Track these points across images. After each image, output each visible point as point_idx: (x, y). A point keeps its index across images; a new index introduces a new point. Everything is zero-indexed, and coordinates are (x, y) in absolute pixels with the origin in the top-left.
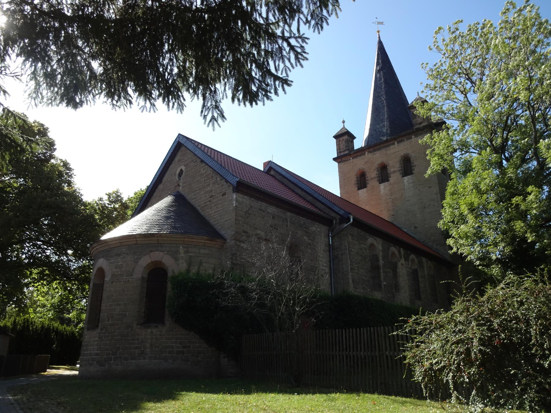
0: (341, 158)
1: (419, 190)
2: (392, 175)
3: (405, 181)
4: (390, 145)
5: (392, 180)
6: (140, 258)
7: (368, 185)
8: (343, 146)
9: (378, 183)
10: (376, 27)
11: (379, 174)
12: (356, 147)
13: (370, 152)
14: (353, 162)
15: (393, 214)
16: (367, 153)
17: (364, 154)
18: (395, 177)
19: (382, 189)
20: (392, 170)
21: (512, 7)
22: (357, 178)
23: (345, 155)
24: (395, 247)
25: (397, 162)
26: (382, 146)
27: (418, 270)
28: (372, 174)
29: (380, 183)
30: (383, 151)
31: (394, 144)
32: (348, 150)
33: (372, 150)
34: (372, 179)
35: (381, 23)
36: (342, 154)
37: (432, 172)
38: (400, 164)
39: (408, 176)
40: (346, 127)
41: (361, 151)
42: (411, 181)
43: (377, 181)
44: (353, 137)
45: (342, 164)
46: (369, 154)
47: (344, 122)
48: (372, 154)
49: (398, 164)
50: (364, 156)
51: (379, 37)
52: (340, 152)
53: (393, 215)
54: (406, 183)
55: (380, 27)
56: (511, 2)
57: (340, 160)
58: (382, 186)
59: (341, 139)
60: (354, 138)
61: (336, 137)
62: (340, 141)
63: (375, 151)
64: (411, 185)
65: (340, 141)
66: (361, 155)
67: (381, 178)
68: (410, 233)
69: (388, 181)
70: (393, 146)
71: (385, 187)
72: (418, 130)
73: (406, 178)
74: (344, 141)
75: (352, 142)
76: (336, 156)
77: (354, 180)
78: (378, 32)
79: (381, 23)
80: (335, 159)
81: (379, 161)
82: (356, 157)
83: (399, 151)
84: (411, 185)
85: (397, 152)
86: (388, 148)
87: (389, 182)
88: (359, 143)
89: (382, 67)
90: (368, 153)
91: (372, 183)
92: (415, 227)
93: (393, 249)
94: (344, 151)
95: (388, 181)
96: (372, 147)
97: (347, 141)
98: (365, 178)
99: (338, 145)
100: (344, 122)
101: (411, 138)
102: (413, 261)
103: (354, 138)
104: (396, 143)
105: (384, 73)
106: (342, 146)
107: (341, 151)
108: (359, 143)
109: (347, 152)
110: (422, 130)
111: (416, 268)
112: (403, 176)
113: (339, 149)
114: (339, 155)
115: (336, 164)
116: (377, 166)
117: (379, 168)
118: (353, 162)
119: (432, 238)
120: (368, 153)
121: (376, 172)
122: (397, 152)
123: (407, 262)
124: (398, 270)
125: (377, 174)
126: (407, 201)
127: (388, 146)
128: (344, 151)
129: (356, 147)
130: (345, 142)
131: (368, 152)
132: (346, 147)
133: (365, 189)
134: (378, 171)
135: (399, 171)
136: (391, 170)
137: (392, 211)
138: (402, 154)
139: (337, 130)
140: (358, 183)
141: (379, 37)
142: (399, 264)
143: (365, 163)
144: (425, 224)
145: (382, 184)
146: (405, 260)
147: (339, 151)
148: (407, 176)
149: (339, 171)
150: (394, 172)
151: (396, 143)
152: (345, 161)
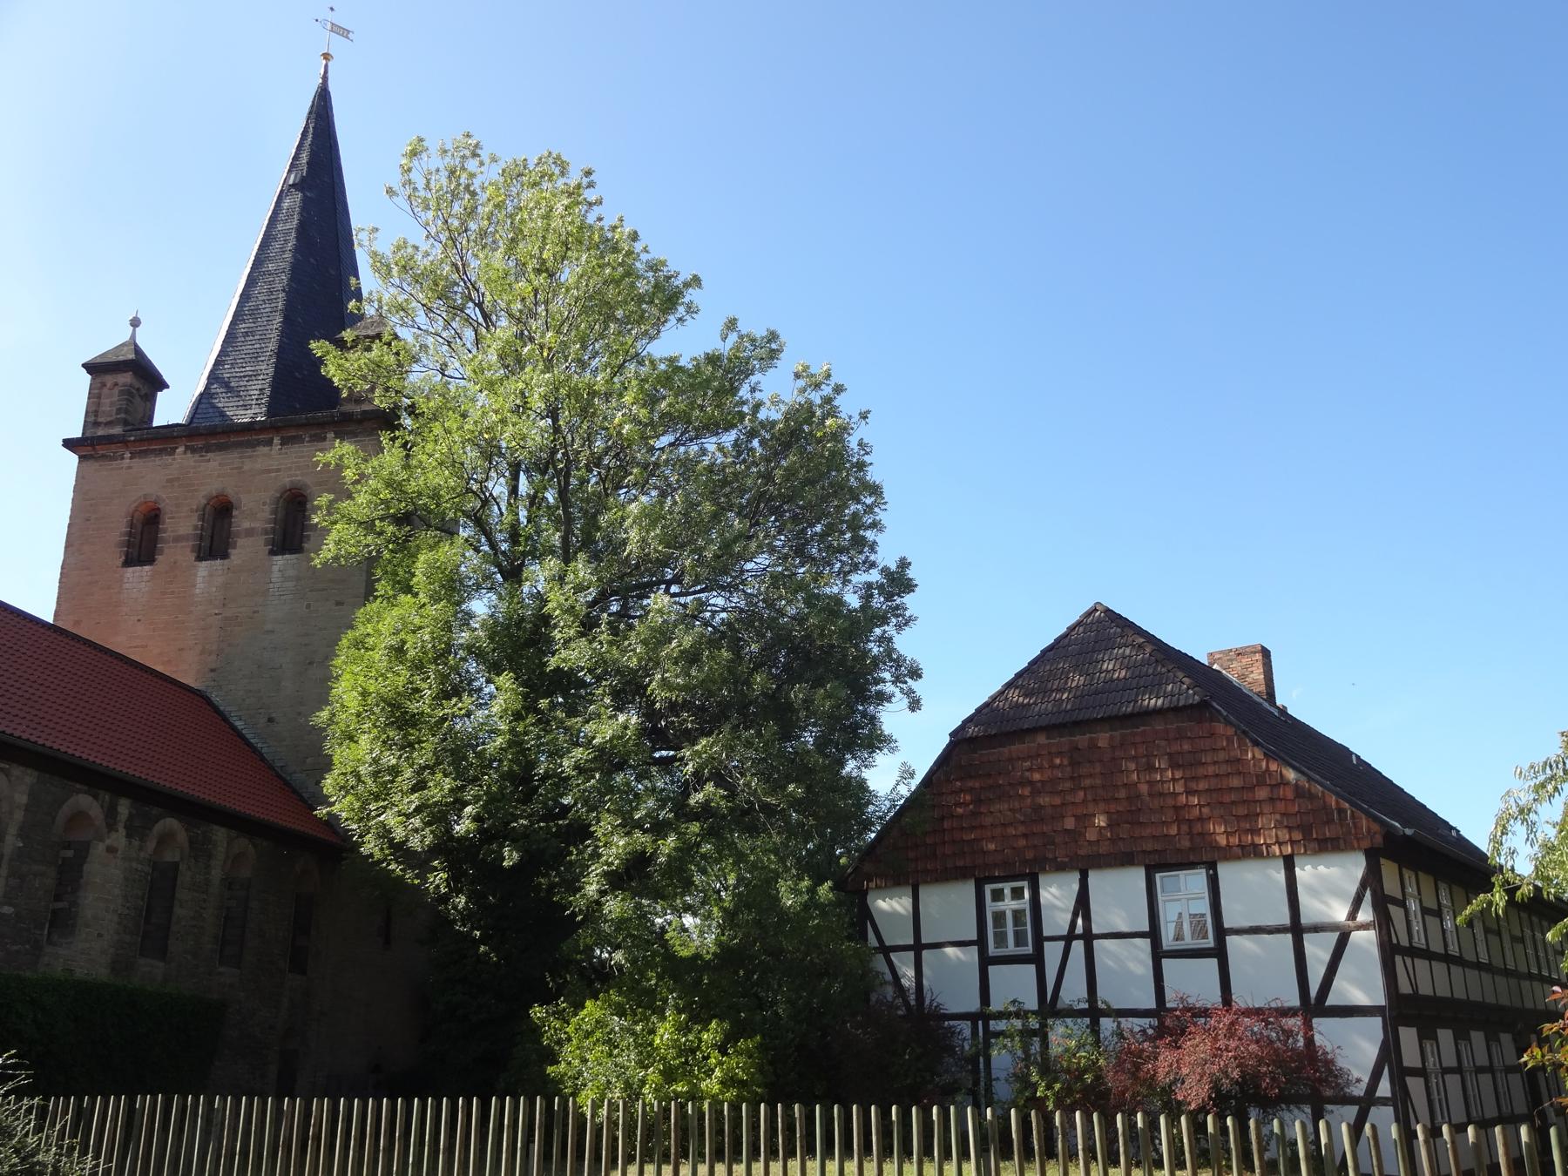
0: (92, 445)
1: (308, 606)
2: (240, 542)
3: (275, 568)
4: (259, 443)
5: (237, 556)
6: (102, 807)
7: (159, 558)
8: (112, 404)
9: (193, 557)
10: (326, 40)
11: (202, 528)
12: (159, 420)
13: (193, 450)
14: (130, 468)
15: (213, 666)
16: (181, 449)
17: (172, 451)
18: (248, 549)
19: (199, 580)
20: (246, 525)
21: (557, 171)
22: (131, 525)
23: (109, 440)
24: (96, 797)
25: (264, 504)
26: (233, 439)
27: (182, 867)
28: (181, 524)
29: (199, 558)
30: (233, 457)
31: (269, 443)
32: (125, 423)
33: (199, 443)
34: (177, 539)
35: (344, 33)
36: (101, 432)
37: (336, 558)
38: (275, 512)
39: (287, 556)
40: (139, 342)
41: (171, 434)
42: (291, 573)
43: (192, 551)
44: (157, 383)
45: (93, 466)
46: (189, 455)
47: (135, 323)
48: (197, 457)
49: (267, 508)
50: (169, 459)
51: (325, 78)
52: (96, 424)
53: (212, 670)
54: (276, 576)
55: (337, 45)
56: (558, 157)
57: (87, 451)
58: (204, 568)
59: (109, 379)
60: (162, 385)
61: (91, 367)
62: (104, 385)
63: (208, 449)
64: (290, 584)
65: (104, 385)
66: (161, 452)
67: (206, 544)
68: (248, 736)
69: (225, 556)
70: (264, 450)
71: (211, 575)
72: (348, 418)
73: (279, 560)
74: (116, 391)
75: (150, 400)
76: (77, 432)
77: (118, 529)
78: (326, 56)
79: (344, 33)
80: (69, 444)
81: (212, 486)
82: (143, 454)
83: (278, 470)
84: (290, 584)
85: (269, 471)
86: (249, 452)
87: (226, 562)
88: (171, 409)
89: (303, 179)
90: (185, 452)
91: (176, 552)
92: (271, 720)
93: (84, 801)
94: (109, 424)
95: (225, 556)
96: (201, 435)
97: (130, 393)
98: (157, 531)
99: (95, 396)
100: (135, 323)
101: (324, 439)
102: (165, 839)
103: (162, 385)
104: (276, 441)
105: (305, 200)
106: (108, 406)
107: (100, 420)
108: (171, 409)
109: (117, 430)
110: (360, 422)
111: (177, 859)
112: (272, 553)
113: (96, 413)
114: (88, 435)
115: (73, 459)
116: (204, 501)
117: (209, 507)
118: (130, 468)
119: (309, 760)
120: (185, 452)
121: (194, 520)
122: (269, 471)
123: (136, 843)
124: (86, 867)
125: (196, 527)
126: (268, 632)
127: (253, 445)
128: (109, 424)
129: (159, 420)
130: (122, 393)
131: (187, 448)
132: (119, 411)
133: (147, 568)
134: (202, 518)
135: (266, 532)
136: (241, 522)
137: (214, 657)
138: (286, 480)
139: (107, 340)
140: (129, 544)
141: (325, 78)
142: (99, 849)
143: (168, 481)
144: (299, 714)
145: (131, 569)
146: (129, 836)
147: (92, 419)
148: (283, 554)
149: (77, 489)
150: (250, 533)
151: (276, 441)
152: (103, 456)
